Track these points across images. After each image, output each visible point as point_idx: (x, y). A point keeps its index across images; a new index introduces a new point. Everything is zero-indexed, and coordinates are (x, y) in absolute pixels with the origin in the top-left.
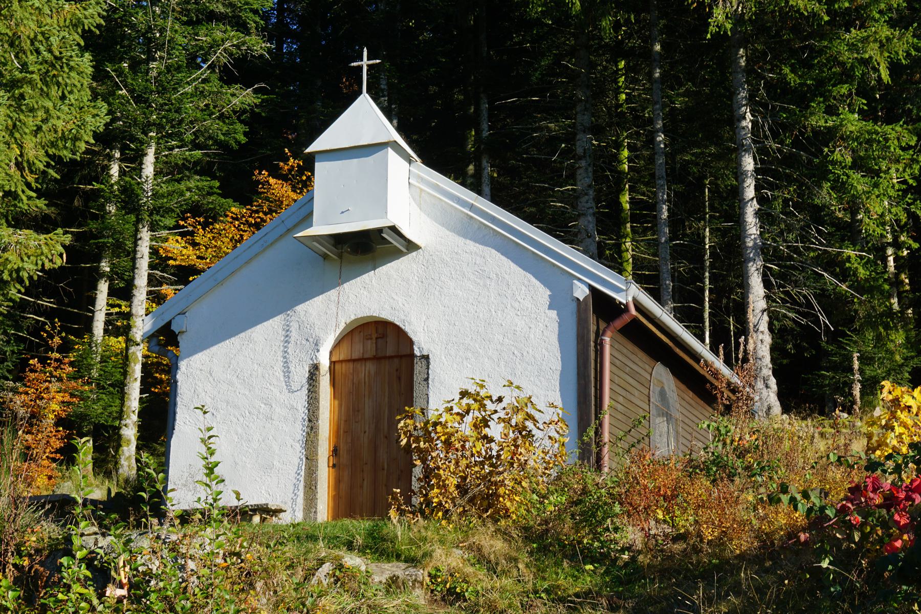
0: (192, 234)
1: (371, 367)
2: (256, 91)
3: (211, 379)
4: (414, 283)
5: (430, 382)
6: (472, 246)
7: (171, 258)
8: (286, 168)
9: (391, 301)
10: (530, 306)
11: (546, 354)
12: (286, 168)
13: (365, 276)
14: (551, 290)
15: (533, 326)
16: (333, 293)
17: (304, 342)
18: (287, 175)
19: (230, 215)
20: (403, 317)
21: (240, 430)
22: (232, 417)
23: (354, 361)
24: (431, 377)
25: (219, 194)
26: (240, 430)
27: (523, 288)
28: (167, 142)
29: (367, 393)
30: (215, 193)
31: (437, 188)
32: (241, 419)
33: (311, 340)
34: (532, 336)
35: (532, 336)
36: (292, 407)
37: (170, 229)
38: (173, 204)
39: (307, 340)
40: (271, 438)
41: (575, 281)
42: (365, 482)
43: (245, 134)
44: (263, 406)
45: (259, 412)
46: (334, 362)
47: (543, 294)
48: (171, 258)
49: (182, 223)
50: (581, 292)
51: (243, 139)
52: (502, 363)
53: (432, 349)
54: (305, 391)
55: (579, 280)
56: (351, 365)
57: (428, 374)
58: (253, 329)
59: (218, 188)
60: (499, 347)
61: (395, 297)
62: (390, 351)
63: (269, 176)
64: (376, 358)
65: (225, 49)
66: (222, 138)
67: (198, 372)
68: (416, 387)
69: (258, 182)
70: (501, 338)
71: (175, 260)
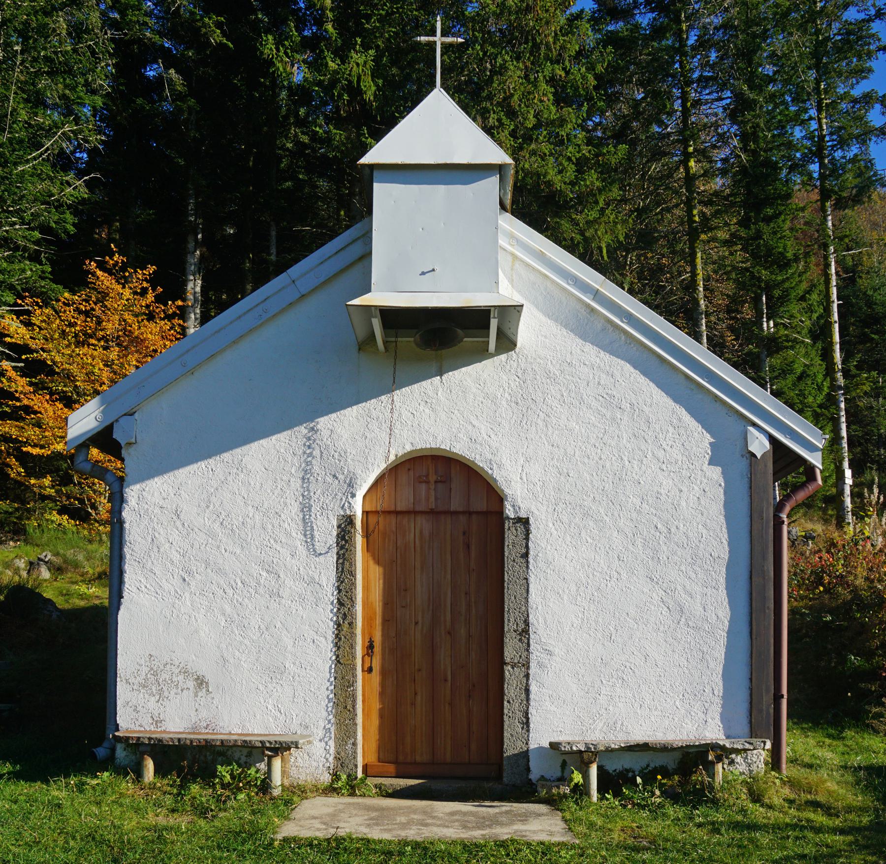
0: (28, 313)
1: (423, 524)
2: (87, 184)
3: (178, 523)
4: (504, 403)
5: (531, 560)
6: (592, 354)
7: (8, 336)
8: (111, 262)
9: (470, 427)
10: (680, 457)
11: (704, 532)
12: (111, 262)
13: (426, 384)
14: (712, 436)
15: (684, 489)
16: (377, 406)
17: (329, 479)
18: (111, 269)
19: (63, 300)
20: (489, 456)
21: (228, 609)
22: (214, 587)
23: (397, 513)
24: (531, 552)
25: (50, 279)
26: (228, 609)
27: (671, 429)
28: (8, 218)
29: (418, 565)
30: (47, 278)
31: (541, 257)
32: (230, 592)
33: (341, 477)
34: (684, 504)
35: (684, 504)
36: (312, 581)
37: (10, 306)
38: (13, 280)
39: (334, 476)
40: (279, 625)
41: (751, 428)
42: (419, 698)
43: (74, 225)
44: (264, 574)
45: (259, 584)
46: (367, 513)
47: (701, 440)
48: (8, 336)
49: (19, 302)
50: (759, 445)
51: (71, 229)
52: (639, 541)
53: (533, 509)
54: (332, 558)
55: (754, 425)
56: (393, 519)
57: (527, 547)
58: (245, 448)
59: (50, 273)
60: (634, 515)
61: (475, 422)
62: (456, 504)
63: (96, 268)
64: (433, 513)
65: (64, 134)
66: (54, 226)
67: (157, 510)
68: (508, 565)
69: (88, 272)
70: (638, 502)
71: (11, 337)
